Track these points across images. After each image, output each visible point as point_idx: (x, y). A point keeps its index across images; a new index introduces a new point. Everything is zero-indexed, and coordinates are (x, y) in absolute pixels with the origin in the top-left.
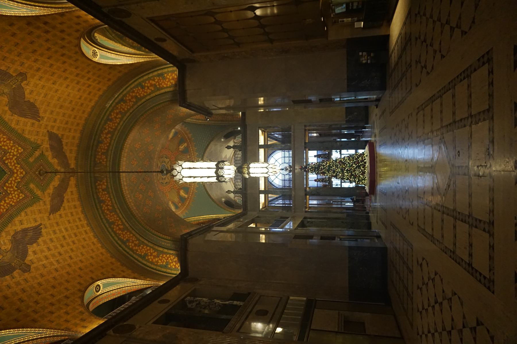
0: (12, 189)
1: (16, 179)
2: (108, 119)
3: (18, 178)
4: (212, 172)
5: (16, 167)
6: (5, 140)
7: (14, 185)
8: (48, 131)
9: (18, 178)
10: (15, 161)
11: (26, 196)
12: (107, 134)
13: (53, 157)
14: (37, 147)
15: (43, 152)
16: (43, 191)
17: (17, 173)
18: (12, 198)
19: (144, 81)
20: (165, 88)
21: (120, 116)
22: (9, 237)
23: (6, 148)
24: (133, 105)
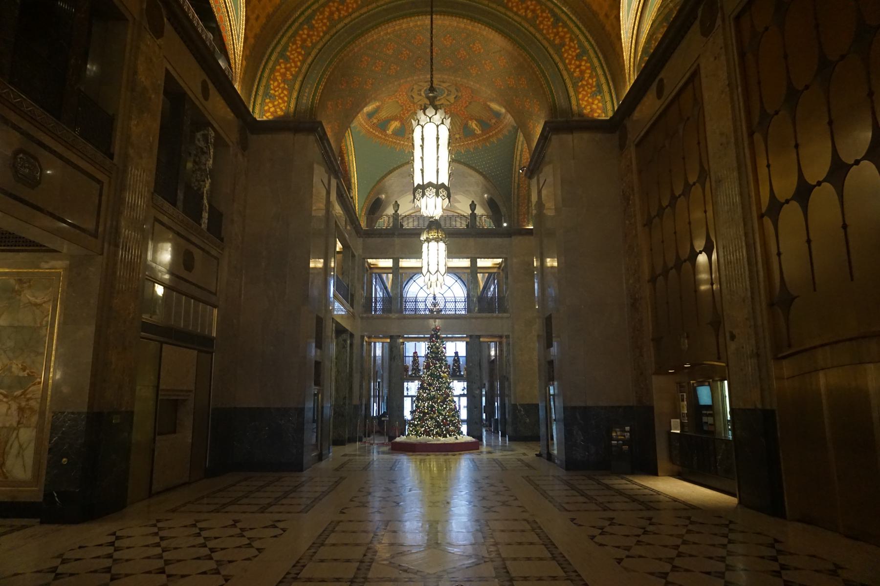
19: (589, 60)
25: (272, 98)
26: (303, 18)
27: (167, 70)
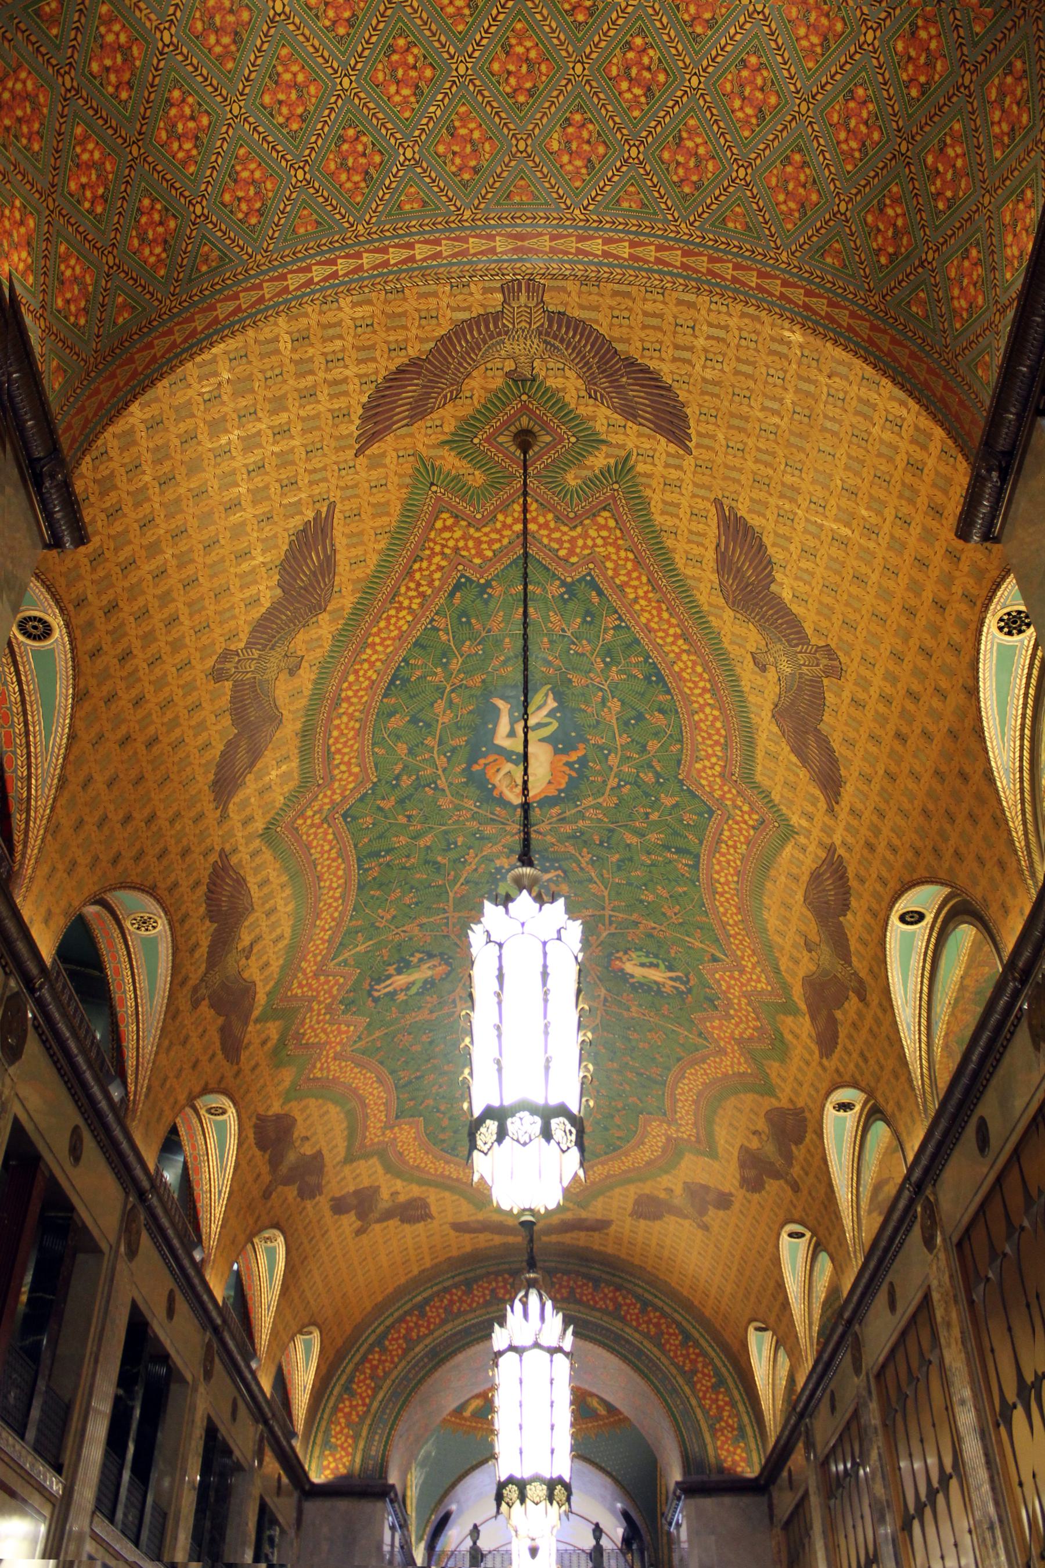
0: (580, 542)
1: (546, 525)
2: (646, 1304)
3: (541, 520)
5: (505, 525)
9: (541, 520)
10: (486, 530)
12: (614, 1300)
14: (426, 472)
16: (594, 441)
19: (728, 1391)
20: (714, 1443)
21: (653, 1330)
24: (676, 1365)
25: (333, 1448)
26: (373, 1338)
27: (16, 1120)
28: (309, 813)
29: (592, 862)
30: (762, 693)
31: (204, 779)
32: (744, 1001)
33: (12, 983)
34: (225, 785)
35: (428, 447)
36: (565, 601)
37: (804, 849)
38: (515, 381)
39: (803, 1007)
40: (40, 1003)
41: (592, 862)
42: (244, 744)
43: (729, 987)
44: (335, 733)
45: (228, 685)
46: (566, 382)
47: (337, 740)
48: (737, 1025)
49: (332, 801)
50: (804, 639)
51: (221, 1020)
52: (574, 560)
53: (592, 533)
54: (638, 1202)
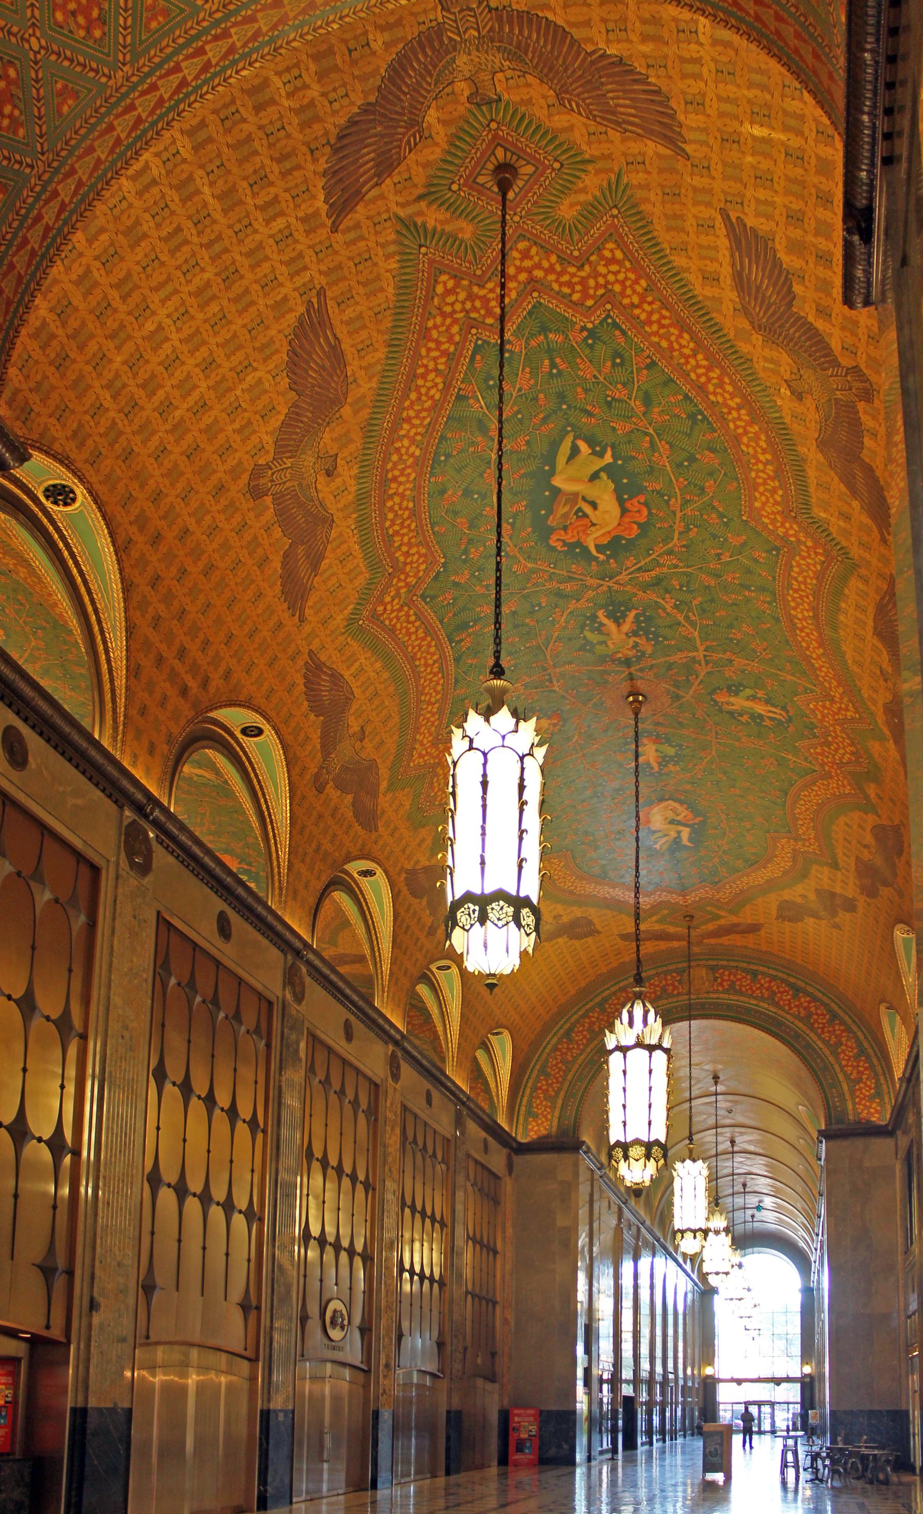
0: (592, 283)
1: (551, 270)
3: (545, 264)
4: (501, 877)
6: (432, 345)
7: (573, 275)
8: (335, 229)
9: (545, 264)
11: (612, 234)
13: (425, 137)
15: (420, 197)
17: (529, 271)
18: (622, 283)
22: (757, 339)
23: (455, 329)
28: (388, 599)
29: (676, 607)
30: (804, 419)
31: (273, 593)
32: (838, 728)
33: (127, 813)
34: (295, 593)
35: (403, 206)
36: (591, 347)
37: (866, 581)
38: (478, 105)
39: (886, 731)
40: (156, 824)
41: (676, 607)
42: (301, 550)
43: (823, 716)
44: (390, 516)
45: (268, 500)
46: (532, 95)
47: (393, 522)
48: (836, 750)
49: (407, 585)
50: (835, 363)
51: (349, 798)
52: (590, 303)
53: (602, 270)
54: (780, 908)
